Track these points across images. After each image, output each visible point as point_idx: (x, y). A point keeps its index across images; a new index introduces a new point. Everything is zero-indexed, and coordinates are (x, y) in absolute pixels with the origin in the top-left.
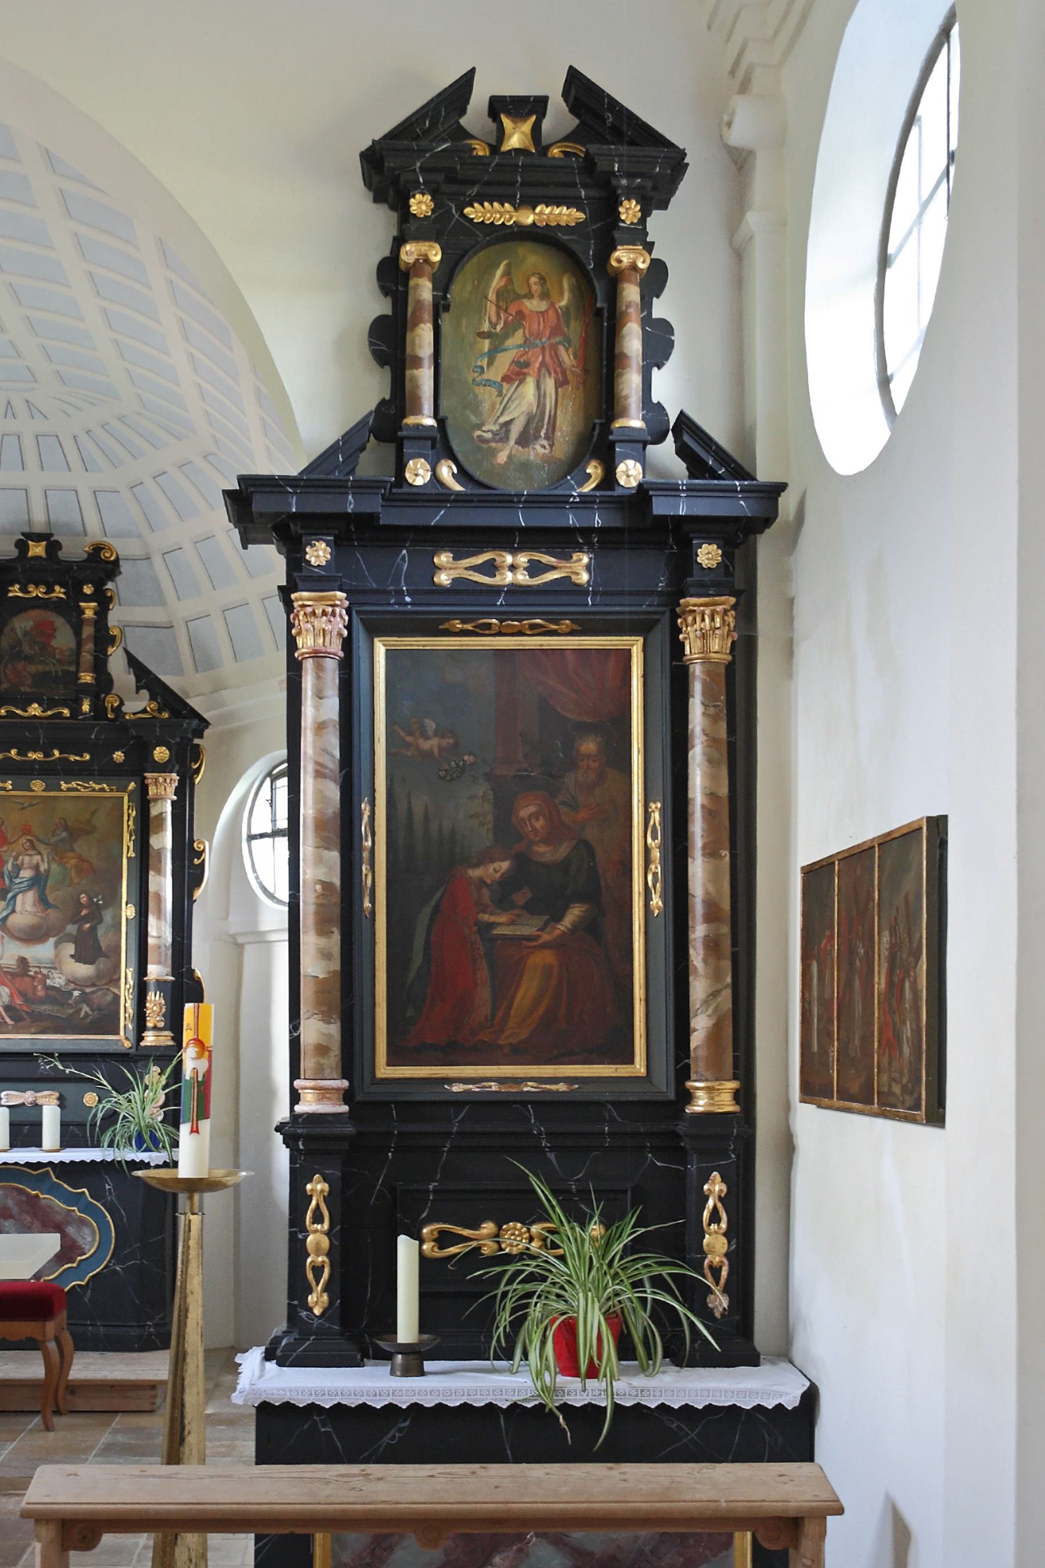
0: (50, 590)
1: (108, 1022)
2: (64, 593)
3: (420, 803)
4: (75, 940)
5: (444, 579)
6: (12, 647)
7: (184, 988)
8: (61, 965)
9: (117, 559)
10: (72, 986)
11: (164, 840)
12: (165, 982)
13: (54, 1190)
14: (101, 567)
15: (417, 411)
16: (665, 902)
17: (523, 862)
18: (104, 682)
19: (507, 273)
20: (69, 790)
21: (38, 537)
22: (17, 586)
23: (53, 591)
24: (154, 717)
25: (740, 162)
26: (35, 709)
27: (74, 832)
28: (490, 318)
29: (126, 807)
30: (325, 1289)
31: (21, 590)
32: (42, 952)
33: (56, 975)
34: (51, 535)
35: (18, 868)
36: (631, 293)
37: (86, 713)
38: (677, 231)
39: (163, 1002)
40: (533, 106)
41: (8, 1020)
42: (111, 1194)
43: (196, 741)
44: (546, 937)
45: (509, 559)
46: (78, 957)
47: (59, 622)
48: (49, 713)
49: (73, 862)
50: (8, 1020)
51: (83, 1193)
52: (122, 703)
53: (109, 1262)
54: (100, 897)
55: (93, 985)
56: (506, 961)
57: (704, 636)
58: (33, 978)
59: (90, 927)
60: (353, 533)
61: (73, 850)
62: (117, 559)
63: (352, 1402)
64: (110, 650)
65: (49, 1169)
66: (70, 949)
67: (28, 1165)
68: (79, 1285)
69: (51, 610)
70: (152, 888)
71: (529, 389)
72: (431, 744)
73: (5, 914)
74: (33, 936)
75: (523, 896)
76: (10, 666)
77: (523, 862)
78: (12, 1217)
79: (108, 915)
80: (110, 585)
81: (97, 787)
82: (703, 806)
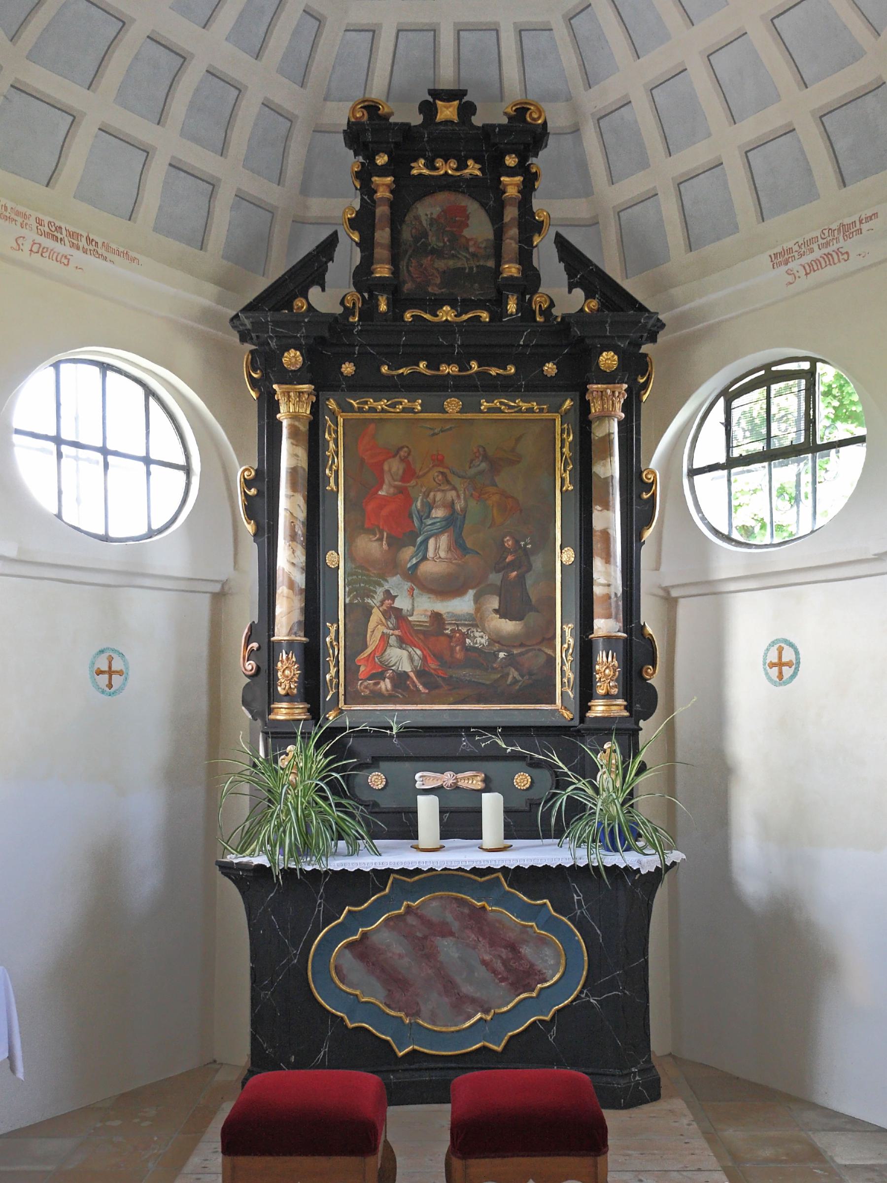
0: (462, 166)
1: (543, 690)
2: (479, 169)
4: (501, 592)
6: (416, 239)
7: (637, 651)
9: (545, 123)
11: (611, 468)
12: (618, 638)
13: (505, 901)
14: (525, 134)
18: (530, 280)
20: (490, 410)
22: (422, 161)
23: (467, 166)
26: (447, 313)
31: (426, 165)
33: (477, 634)
34: (464, 93)
35: (430, 507)
37: (511, 315)
39: (616, 663)
41: (421, 687)
42: (580, 906)
46: (503, 612)
47: (473, 207)
48: (465, 317)
49: (496, 498)
50: (421, 687)
51: (545, 904)
53: (581, 992)
54: (528, 540)
55: (522, 645)
59: (517, 576)
61: (494, 484)
64: (536, 240)
65: (500, 875)
67: (475, 871)
68: (541, 1021)
70: (598, 524)
73: (414, 561)
74: (447, 587)
76: (414, 262)
78: (452, 934)
79: (537, 562)
80: (532, 160)
81: (524, 406)
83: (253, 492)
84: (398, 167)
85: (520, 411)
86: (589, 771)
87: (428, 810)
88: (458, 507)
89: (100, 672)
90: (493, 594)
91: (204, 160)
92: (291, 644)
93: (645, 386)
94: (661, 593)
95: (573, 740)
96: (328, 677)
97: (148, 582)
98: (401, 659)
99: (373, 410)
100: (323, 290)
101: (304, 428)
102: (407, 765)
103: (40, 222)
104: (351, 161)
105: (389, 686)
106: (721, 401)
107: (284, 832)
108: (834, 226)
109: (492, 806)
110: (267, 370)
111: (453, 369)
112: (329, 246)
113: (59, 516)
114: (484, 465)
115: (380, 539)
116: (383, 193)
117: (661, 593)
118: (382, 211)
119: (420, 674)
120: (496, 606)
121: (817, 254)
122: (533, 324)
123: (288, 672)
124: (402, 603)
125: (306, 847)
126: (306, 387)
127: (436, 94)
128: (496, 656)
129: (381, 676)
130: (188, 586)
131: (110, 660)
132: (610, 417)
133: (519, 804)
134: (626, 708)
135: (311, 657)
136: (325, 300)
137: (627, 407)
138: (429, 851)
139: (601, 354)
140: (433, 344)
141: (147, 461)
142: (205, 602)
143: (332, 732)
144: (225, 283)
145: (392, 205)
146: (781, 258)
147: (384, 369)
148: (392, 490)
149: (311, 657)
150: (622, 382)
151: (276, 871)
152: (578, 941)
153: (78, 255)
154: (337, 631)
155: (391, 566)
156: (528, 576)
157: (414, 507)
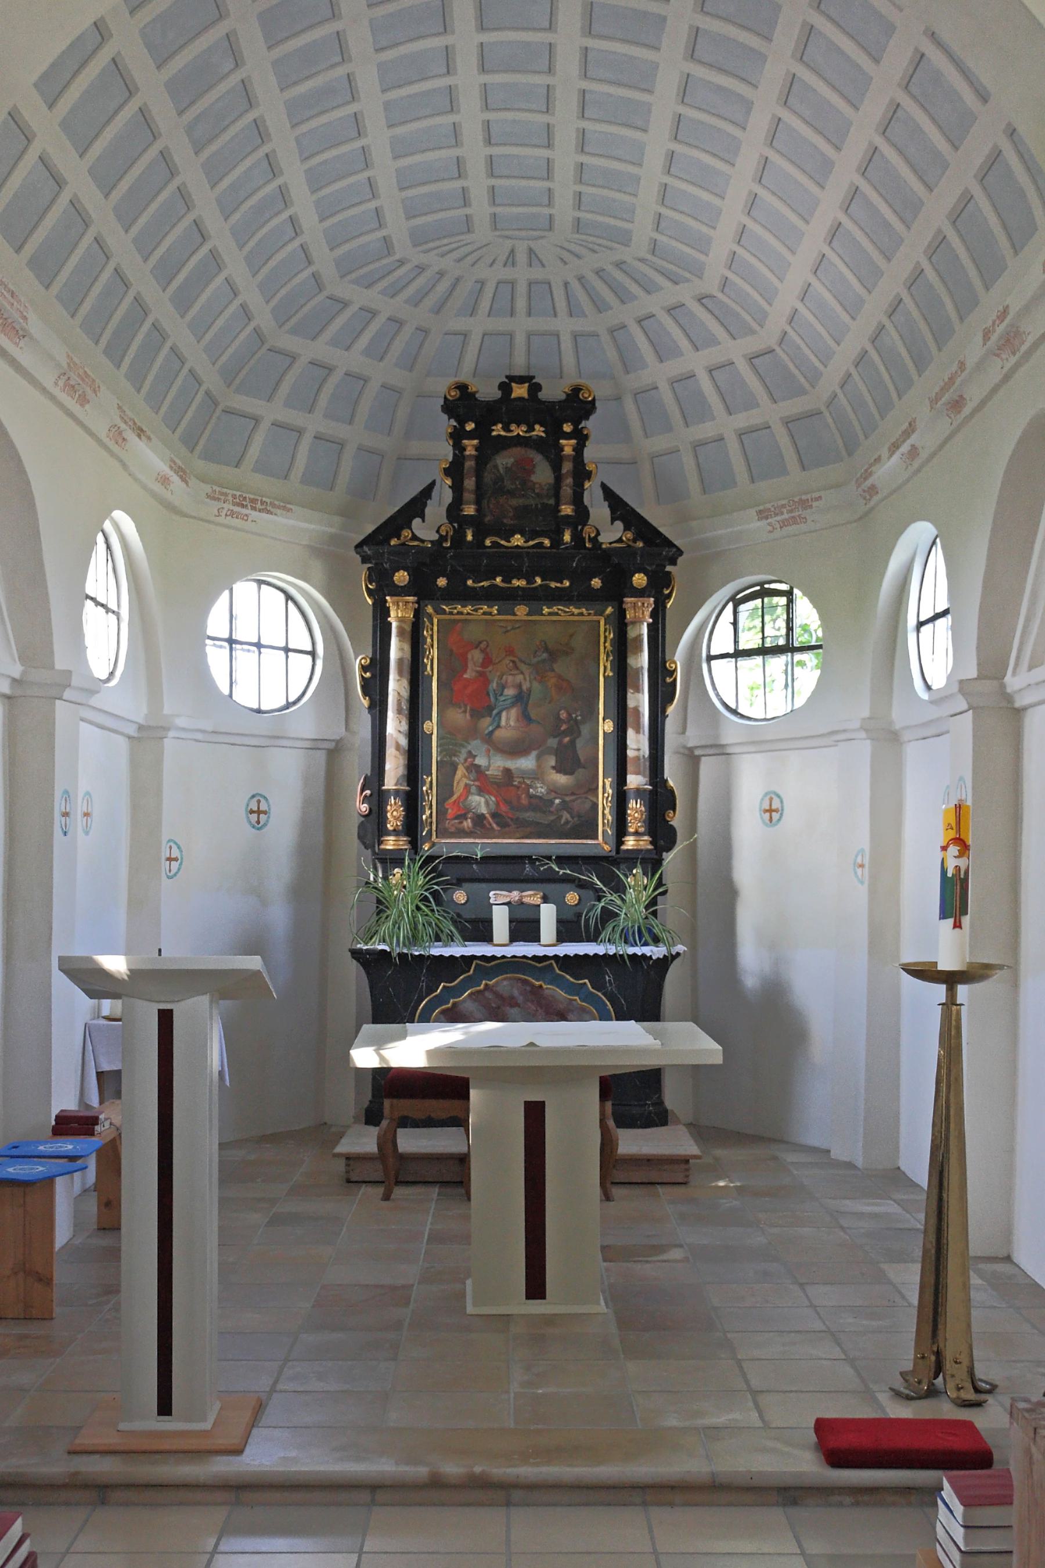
0: (531, 429)
1: (587, 827)
4: (558, 752)
7: (660, 799)
8: (540, 773)
9: (594, 400)
10: (553, 795)
12: (645, 790)
13: (557, 981)
14: (578, 406)
18: (582, 514)
20: (550, 614)
21: (521, 380)
22: (500, 426)
23: (534, 430)
24: (629, 546)
26: (518, 540)
29: (602, 629)
31: (503, 428)
32: (526, 763)
34: (533, 377)
39: (643, 809)
43: (668, 568)
46: (558, 769)
47: (538, 458)
48: (531, 543)
49: (553, 681)
50: (495, 826)
52: (598, 534)
55: (573, 794)
58: (518, 788)
61: (553, 670)
62: (594, 400)
64: (587, 485)
65: (553, 962)
66: (552, 761)
69: (531, 447)
70: (631, 703)
73: (491, 728)
74: (516, 749)
76: (493, 501)
78: (517, 1005)
79: (585, 730)
81: (576, 611)
83: (368, 675)
84: (482, 432)
85: (573, 615)
86: (620, 888)
87: (500, 919)
88: (524, 688)
89: (252, 812)
90: (550, 754)
91: (339, 430)
92: (397, 793)
93: (669, 596)
94: (686, 752)
95: (610, 866)
96: (424, 817)
97: (285, 743)
98: (480, 803)
99: (460, 613)
100: (423, 521)
101: (408, 628)
102: (484, 885)
103: (234, 497)
104: (446, 424)
105: (470, 825)
106: (731, 605)
107: (399, 928)
108: (796, 499)
109: (548, 915)
110: (382, 587)
111: (521, 583)
112: (427, 492)
113: (231, 695)
114: (545, 655)
115: (465, 712)
116: (470, 451)
117: (686, 752)
118: (470, 464)
119: (494, 815)
120: (553, 763)
121: (786, 516)
122: (582, 551)
123: (394, 813)
125: (414, 939)
126: (411, 599)
127: (512, 379)
128: (553, 803)
129: (463, 817)
130: (315, 745)
131: (259, 802)
132: (642, 622)
133: (569, 916)
134: (651, 843)
135: (412, 801)
136: (426, 530)
137: (654, 614)
138: (501, 945)
139: (633, 575)
140: (509, 563)
141: (287, 650)
142: (321, 757)
143: (430, 859)
144: (348, 513)
145: (477, 458)
146: (763, 515)
147: (470, 582)
148: (474, 674)
149: (412, 801)
150: (649, 596)
151: (394, 954)
152: (609, 1010)
153: (255, 514)
154: (431, 782)
155: (473, 732)
156: (578, 741)
157: (490, 687)
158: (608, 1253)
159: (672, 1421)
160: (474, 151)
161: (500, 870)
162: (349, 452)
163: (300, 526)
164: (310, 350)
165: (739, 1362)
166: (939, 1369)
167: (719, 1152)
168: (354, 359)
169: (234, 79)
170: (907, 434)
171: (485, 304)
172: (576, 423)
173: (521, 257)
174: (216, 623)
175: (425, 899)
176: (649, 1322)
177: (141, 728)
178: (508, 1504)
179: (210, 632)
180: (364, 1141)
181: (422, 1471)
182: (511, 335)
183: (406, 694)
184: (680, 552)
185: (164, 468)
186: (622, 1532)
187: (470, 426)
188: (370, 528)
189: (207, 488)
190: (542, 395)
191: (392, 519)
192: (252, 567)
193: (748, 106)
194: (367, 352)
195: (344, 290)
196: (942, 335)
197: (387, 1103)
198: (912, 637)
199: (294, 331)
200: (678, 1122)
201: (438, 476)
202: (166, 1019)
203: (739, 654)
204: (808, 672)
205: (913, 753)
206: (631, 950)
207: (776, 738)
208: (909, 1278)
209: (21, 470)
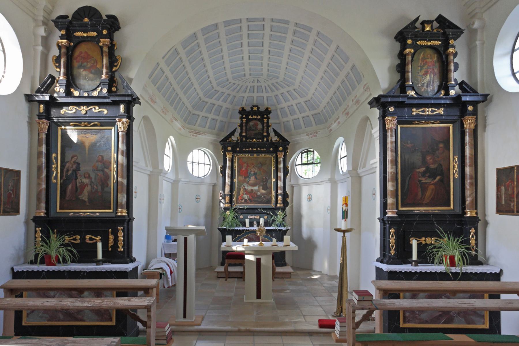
1: (269, 202)
3: (407, 157)
5: (414, 113)
7: (285, 196)
14: (268, 112)
15: (408, 81)
16: (459, 175)
17: (428, 168)
18: (268, 135)
19: (424, 54)
21: (255, 106)
25: (473, 32)
27: (262, 164)
28: (420, 63)
30: (394, 250)
32: (256, 188)
35: (251, 172)
36: (452, 57)
38: (458, 46)
40: (429, 22)
44: (432, 183)
45: (427, 110)
46: (263, 189)
47: (259, 123)
56: (424, 188)
57: (470, 124)
60: (399, 105)
63: (408, 271)
66: (262, 188)
71: (428, 76)
72: (409, 145)
74: (254, 185)
75: (427, 175)
77: (428, 168)
79: (269, 181)
82: (469, 157)
84: (247, 117)
86: (276, 215)
91: (215, 117)
92: (228, 195)
95: (274, 210)
98: (246, 197)
109: (262, 221)
110: (225, 150)
112: (235, 130)
118: (244, 124)
124: (246, 188)
125: (232, 226)
127: (253, 106)
129: (242, 200)
134: (45, 213)
136: (234, 138)
142: (211, 187)
143: (235, 209)
144: (218, 135)
146: (308, 135)
155: (244, 181)
158: (273, 291)
159: (287, 320)
160: (246, 61)
161: (249, 211)
162: (218, 122)
163: (209, 138)
164: (210, 101)
165: (301, 311)
166: (342, 311)
167: (298, 272)
168: (220, 103)
169: (198, 50)
170: (338, 119)
171: (248, 91)
172: (267, 115)
173: (256, 81)
174: (190, 158)
175: (234, 217)
176: (282, 304)
177: (174, 181)
178: (254, 335)
179: (188, 160)
180: (222, 269)
181: (236, 329)
182: (253, 97)
183: (230, 173)
184: (290, 143)
185: (180, 127)
186: (276, 340)
187: (244, 116)
188: (222, 138)
189: (188, 130)
190: (260, 109)
191: (227, 136)
192: (197, 146)
193: (304, 53)
194: (223, 101)
195: (218, 88)
196: (344, 99)
197: (226, 260)
198: (339, 161)
199: (207, 97)
200: (288, 265)
201: (237, 127)
202: (186, 239)
203: (302, 164)
204: (318, 168)
205: (339, 185)
206: (279, 228)
207: (310, 183)
208: (336, 295)
209: (154, 129)
